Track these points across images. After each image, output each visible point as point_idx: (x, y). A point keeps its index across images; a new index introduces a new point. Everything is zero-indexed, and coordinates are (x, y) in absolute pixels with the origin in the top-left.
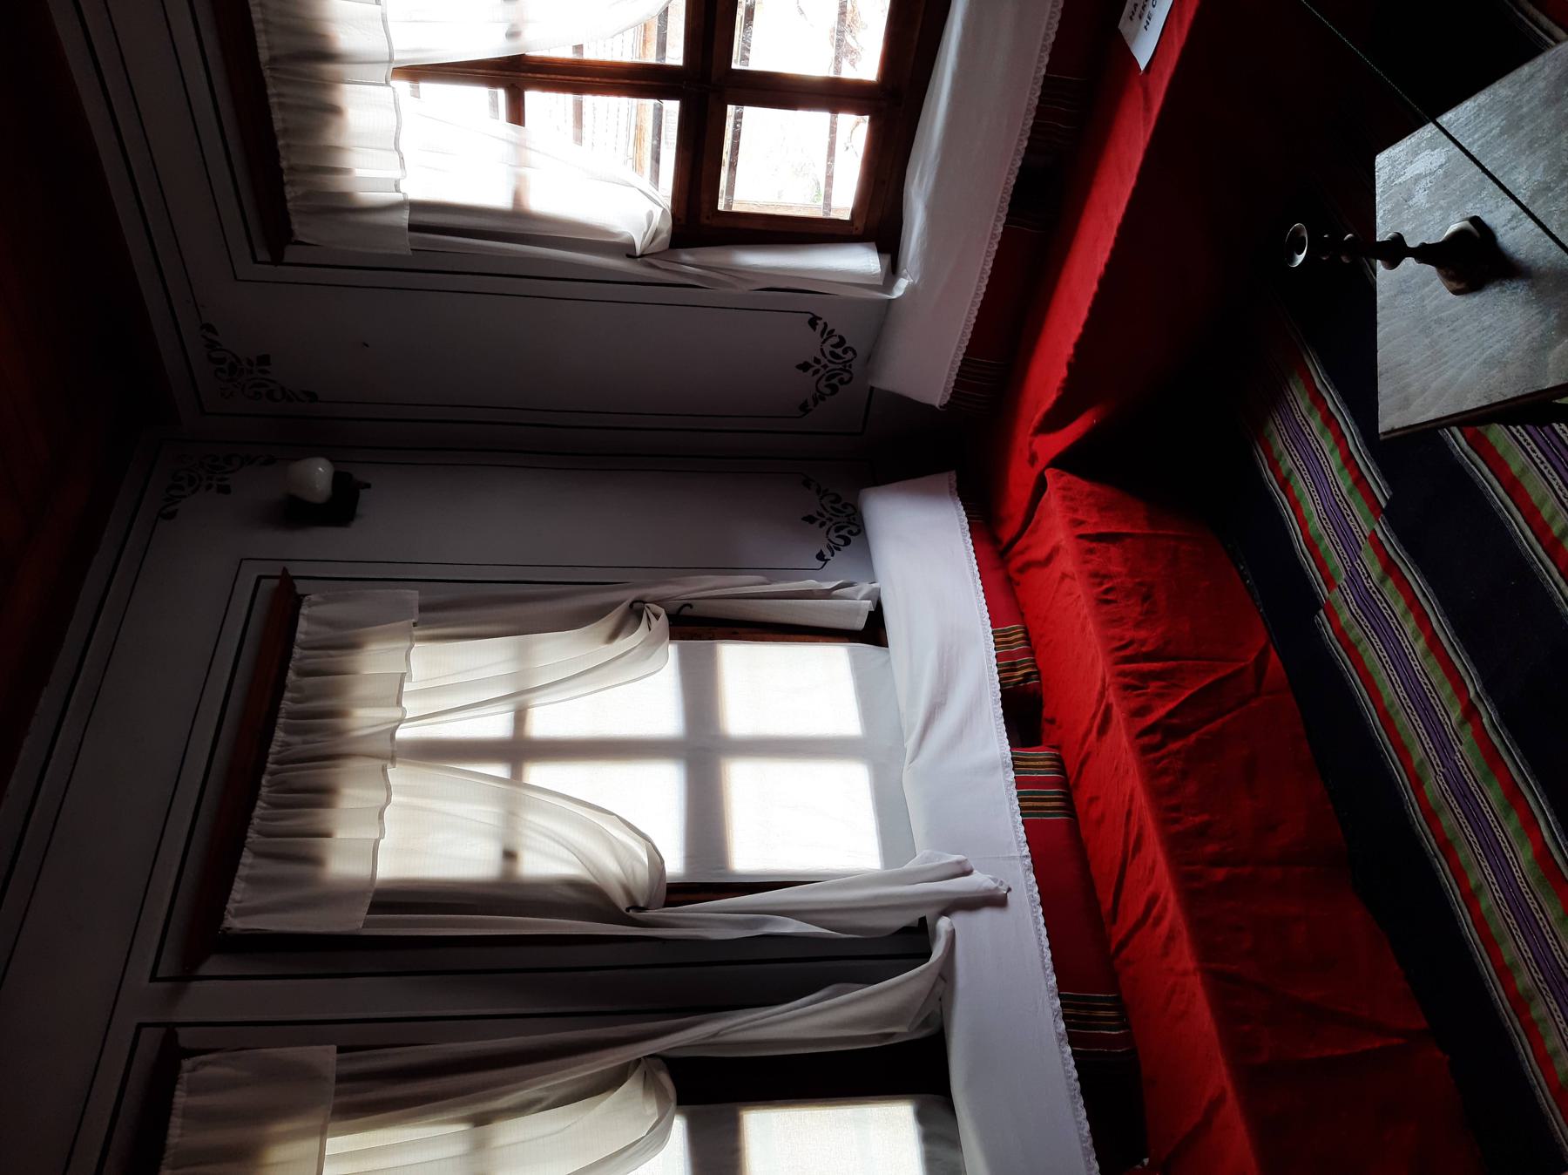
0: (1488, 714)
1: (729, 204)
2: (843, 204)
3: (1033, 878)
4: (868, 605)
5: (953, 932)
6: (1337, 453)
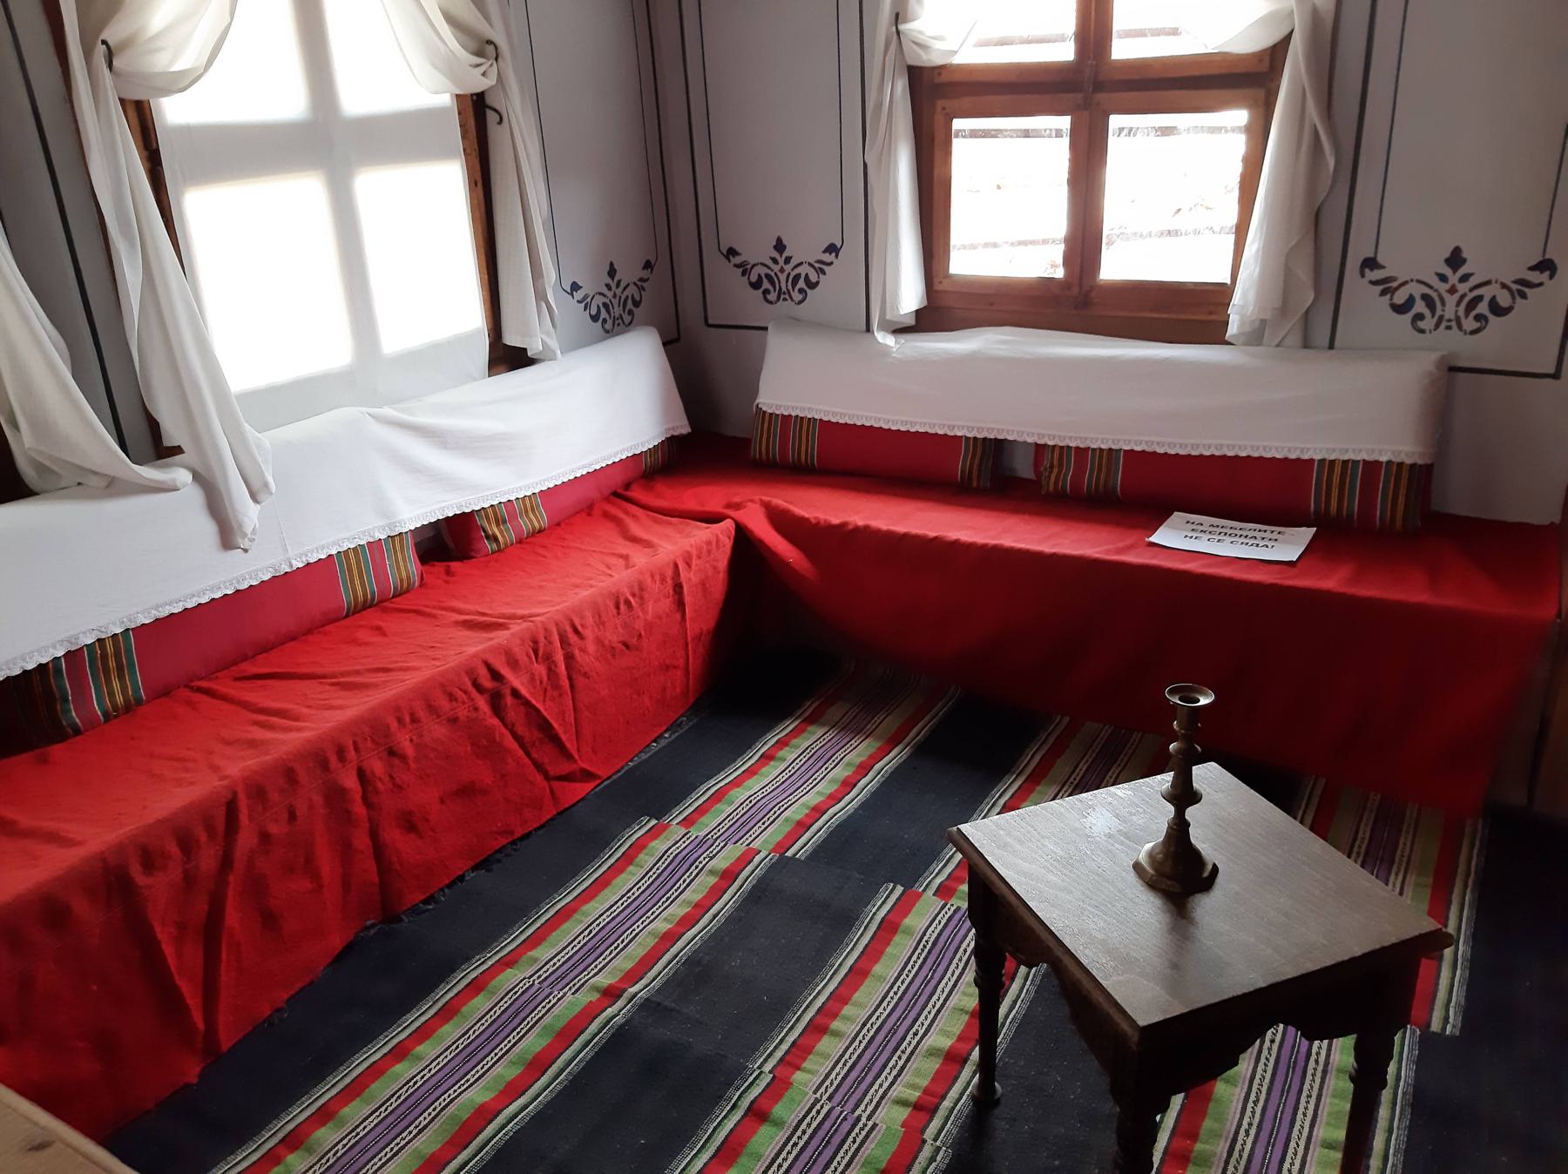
0: (617, 1011)
2: (964, 263)
5: (175, 489)
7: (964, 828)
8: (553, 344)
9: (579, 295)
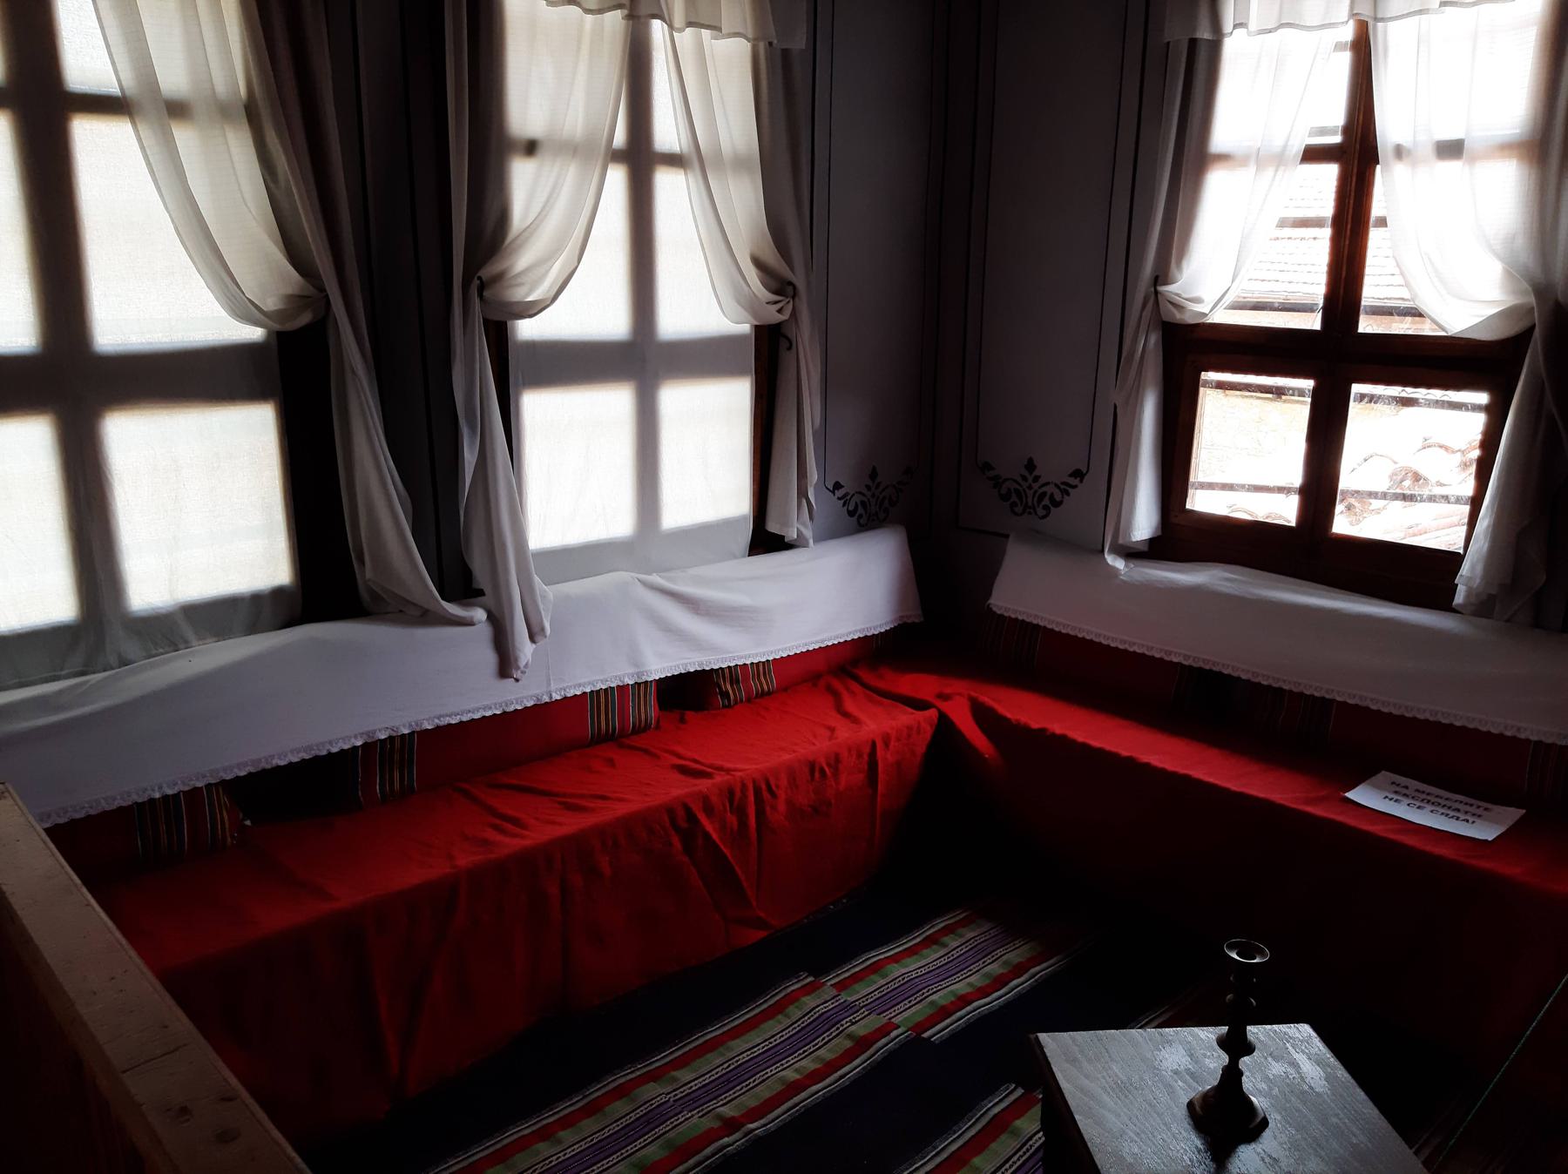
0: (732, 1142)
1: (1208, 384)
2: (1200, 502)
3: (530, 704)
4: (791, 534)
6: (969, 990)
7: (1044, 1037)
8: (808, 533)
9: (839, 493)
